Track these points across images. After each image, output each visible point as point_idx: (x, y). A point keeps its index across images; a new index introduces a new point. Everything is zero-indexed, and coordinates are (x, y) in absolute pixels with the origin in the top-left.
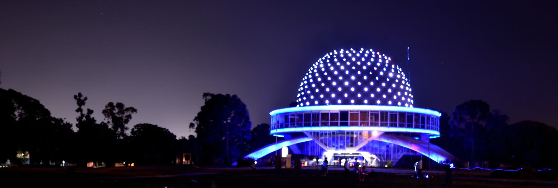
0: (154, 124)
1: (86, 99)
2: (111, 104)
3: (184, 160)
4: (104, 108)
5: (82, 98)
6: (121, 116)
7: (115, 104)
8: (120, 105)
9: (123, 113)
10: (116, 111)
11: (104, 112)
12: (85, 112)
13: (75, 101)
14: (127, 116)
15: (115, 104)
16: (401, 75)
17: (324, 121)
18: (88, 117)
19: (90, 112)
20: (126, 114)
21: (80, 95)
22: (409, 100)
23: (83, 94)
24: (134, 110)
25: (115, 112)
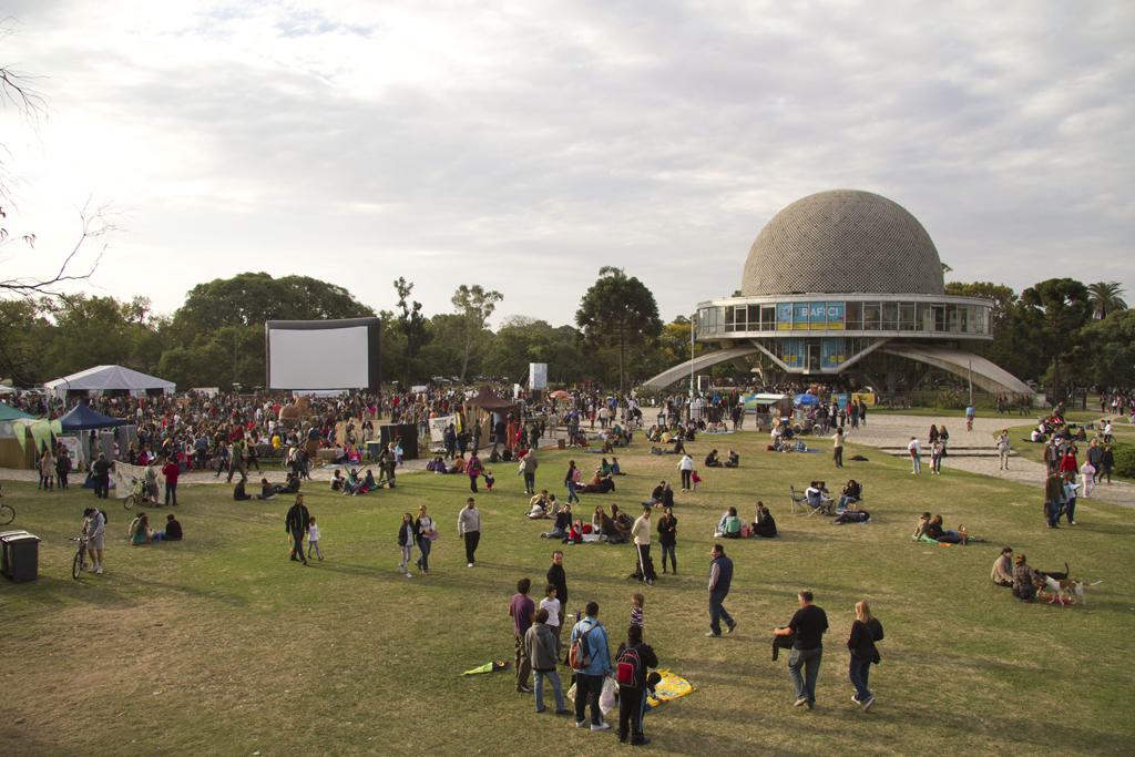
0: (943, 260)
1: (411, 286)
2: (464, 288)
3: (1077, 347)
4: (453, 294)
5: (407, 285)
6: (478, 305)
7: (470, 288)
8: (477, 290)
9: (482, 302)
10: (471, 297)
11: (454, 300)
12: (410, 307)
13: (396, 291)
14: (488, 306)
15: (470, 288)
16: (601, 708)
17: (554, 384)
18: (415, 314)
19: (418, 306)
20: (488, 300)
21: (402, 280)
22: (810, 548)
23: (405, 279)
24: (498, 296)
25: (469, 299)
